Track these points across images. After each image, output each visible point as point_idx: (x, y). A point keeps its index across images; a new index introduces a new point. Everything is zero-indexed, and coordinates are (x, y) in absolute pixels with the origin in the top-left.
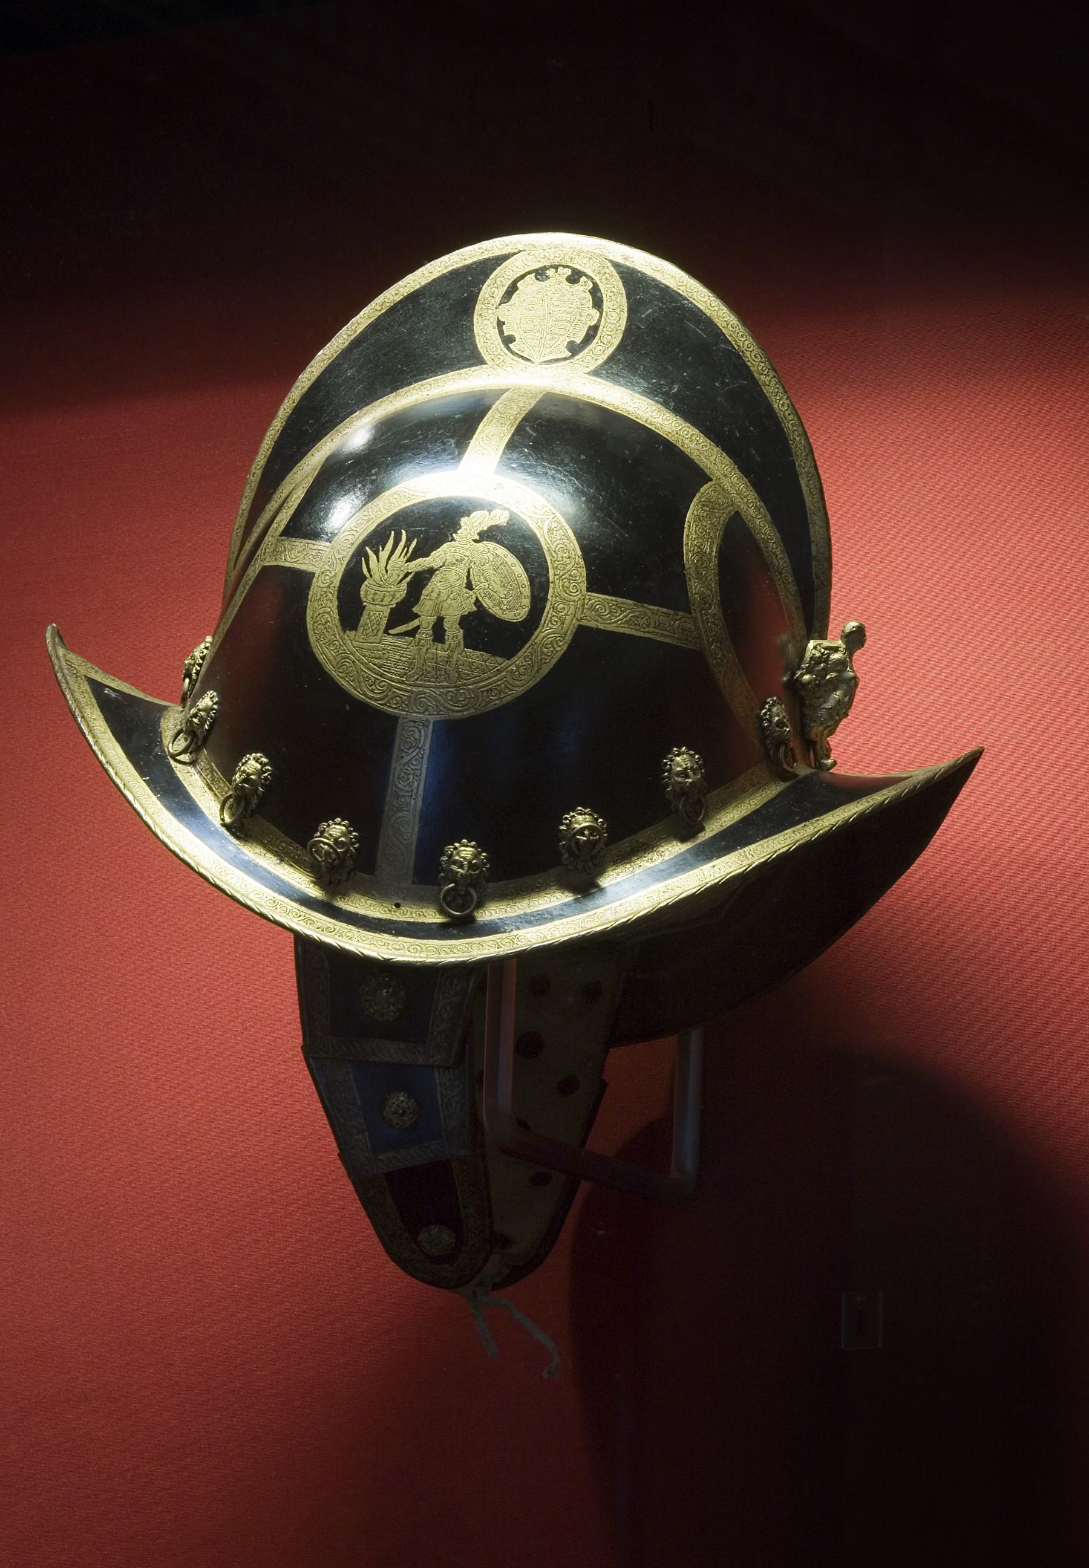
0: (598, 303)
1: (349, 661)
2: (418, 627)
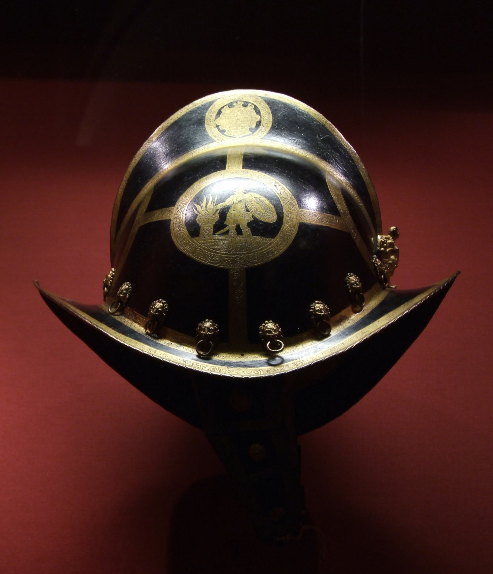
0: (258, 112)
1: (198, 250)
2: (228, 230)
